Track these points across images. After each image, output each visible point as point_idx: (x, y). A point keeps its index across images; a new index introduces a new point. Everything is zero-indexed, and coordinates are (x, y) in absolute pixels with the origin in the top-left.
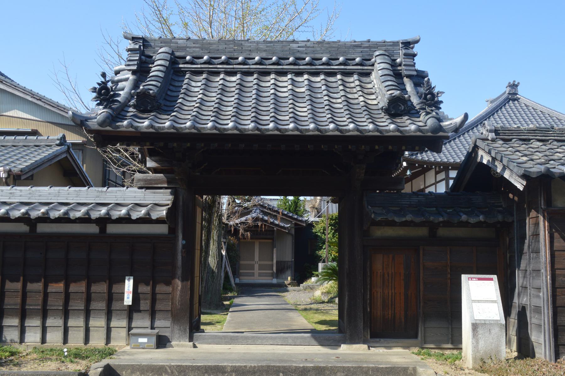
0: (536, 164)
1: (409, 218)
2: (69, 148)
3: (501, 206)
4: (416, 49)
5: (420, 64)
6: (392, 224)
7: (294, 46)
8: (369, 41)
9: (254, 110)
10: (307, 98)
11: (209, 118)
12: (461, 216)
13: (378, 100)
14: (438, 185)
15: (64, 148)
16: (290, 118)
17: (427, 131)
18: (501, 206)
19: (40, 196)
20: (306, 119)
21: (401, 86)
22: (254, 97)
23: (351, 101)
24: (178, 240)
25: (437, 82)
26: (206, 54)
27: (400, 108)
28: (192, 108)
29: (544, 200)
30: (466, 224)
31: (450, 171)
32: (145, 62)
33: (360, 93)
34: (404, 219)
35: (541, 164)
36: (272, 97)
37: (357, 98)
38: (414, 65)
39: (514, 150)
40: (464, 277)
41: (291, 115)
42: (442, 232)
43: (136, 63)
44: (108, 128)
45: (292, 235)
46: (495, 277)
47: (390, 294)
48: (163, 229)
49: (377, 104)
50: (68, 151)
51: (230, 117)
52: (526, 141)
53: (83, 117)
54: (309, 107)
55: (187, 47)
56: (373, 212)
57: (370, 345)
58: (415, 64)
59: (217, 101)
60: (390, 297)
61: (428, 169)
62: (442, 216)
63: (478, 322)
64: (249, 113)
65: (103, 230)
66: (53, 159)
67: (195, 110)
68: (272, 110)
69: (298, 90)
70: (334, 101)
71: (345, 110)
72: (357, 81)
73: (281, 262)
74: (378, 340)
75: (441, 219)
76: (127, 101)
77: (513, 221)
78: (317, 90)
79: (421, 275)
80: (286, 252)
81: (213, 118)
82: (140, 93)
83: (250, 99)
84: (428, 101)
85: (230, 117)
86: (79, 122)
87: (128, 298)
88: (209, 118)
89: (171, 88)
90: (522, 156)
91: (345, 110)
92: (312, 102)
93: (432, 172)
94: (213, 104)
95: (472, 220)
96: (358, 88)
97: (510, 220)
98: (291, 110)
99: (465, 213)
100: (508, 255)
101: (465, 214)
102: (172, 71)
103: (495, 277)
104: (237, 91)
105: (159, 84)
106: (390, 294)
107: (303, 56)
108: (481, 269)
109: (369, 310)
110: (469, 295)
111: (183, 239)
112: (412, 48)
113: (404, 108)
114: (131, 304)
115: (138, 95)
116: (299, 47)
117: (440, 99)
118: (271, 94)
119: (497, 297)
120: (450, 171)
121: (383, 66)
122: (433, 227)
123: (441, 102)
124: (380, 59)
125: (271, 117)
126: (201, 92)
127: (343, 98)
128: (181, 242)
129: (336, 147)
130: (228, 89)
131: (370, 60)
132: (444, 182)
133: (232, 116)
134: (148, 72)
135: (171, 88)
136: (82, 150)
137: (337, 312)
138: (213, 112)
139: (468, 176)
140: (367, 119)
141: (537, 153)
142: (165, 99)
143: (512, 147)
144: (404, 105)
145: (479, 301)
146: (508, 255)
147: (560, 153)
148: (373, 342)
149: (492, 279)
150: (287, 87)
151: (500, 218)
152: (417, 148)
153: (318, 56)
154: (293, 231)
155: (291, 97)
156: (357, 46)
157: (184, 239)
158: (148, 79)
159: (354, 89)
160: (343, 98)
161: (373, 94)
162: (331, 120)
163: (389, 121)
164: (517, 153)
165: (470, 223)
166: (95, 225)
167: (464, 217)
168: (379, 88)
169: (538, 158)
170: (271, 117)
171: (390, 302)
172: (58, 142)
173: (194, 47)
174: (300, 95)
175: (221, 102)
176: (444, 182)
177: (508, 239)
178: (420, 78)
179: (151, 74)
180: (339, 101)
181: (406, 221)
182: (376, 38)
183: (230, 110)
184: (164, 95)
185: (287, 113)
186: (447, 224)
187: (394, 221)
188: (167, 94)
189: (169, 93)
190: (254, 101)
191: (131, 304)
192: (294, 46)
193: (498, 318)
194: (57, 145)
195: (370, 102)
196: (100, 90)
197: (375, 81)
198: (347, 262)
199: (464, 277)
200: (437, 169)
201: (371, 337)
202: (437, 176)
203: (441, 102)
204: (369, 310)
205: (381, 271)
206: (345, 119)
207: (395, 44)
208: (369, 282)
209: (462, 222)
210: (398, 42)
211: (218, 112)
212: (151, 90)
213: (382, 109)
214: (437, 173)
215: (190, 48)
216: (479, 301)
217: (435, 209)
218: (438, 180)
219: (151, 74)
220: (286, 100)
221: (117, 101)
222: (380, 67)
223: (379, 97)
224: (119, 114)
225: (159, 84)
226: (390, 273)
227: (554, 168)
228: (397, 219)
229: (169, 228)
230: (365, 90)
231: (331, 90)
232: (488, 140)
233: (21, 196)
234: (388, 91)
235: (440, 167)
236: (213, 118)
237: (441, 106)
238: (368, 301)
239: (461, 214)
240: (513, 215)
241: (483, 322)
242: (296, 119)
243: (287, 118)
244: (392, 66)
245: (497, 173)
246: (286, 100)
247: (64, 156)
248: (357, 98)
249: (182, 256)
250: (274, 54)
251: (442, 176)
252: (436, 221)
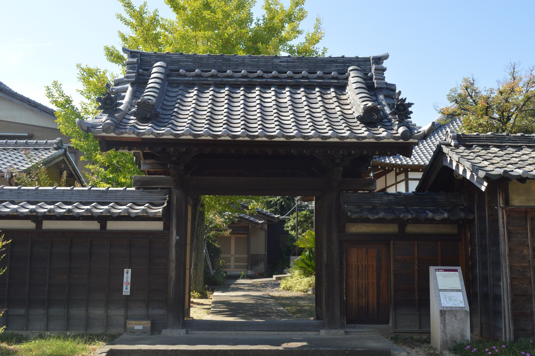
0: (496, 168)
1: (381, 215)
2: (65, 151)
3: (463, 205)
4: (385, 64)
5: (389, 78)
6: (366, 221)
7: (277, 61)
8: (343, 57)
9: (243, 118)
10: (290, 107)
11: (203, 125)
12: (427, 214)
13: (353, 110)
14: (398, 185)
15: (61, 151)
16: (276, 125)
17: (398, 138)
18: (463, 205)
19: (46, 196)
20: (290, 126)
21: (376, 100)
22: (242, 106)
23: (330, 111)
24: (172, 236)
25: (406, 93)
26: (197, 68)
27: (374, 117)
28: (187, 116)
29: (503, 200)
30: (432, 221)
31: (409, 173)
32: (142, 75)
33: (337, 104)
34: (376, 217)
35: (500, 168)
36: (258, 106)
37: (334, 108)
38: (384, 79)
39: (475, 155)
40: (432, 269)
41: (277, 123)
42: (411, 229)
43: (134, 74)
44: (112, 135)
45: (265, 230)
46: (459, 268)
47: (364, 284)
48: (158, 226)
49: (352, 114)
50: (65, 154)
51: (221, 125)
52: (486, 147)
53: (90, 124)
54: (292, 116)
55: (180, 61)
56: (349, 210)
57: (346, 330)
58: (384, 77)
59: (209, 110)
60: (364, 287)
61: (389, 171)
62: (411, 214)
63: (445, 309)
64: (239, 121)
65: (103, 226)
66: (51, 161)
67: (190, 118)
68: (259, 119)
69: (281, 100)
70: (314, 110)
71: (324, 119)
72: (334, 93)
73: (255, 255)
74: (353, 325)
75: (410, 217)
76: (127, 110)
77: (474, 219)
78: (297, 101)
79: (392, 267)
80: (259, 245)
81: (207, 126)
82: (140, 102)
83: (238, 109)
84: (400, 111)
85: (221, 125)
86: (86, 129)
87: (126, 289)
88: (203, 125)
89: (167, 98)
90: (483, 161)
91: (324, 119)
92: (295, 113)
93: (393, 173)
94: (205, 112)
95: (438, 217)
96: (335, 99)
97: (471, 217)
98: (276, 119)
99: (431, 211)
100: (470, 249)
101: (431, 212)
102: (167, 82)
103: (459, 268)
104: (226, 101)
105: (156, 95)
106: (364, 284)
107: (285, 69)
108: (448, 262)
109: (345, 298)
110: (437, 285)
111: (177, 235)
112: (382, 63)
113: (378, 117)
114: (129, 294)
115: (138, 104)
116: (281, 62)
117: (410, 109)
118: (257, 104)
119: (462, 286)
120: (409, 173)
121: (356, 79)
122: (402, 224)
123: (411, 112)
124: (354, 73)
125: (259, 125)
126: (194, 101)
127: (322, 108)
128: (175, 237)
129: (317, 152)
130: (218, 100)
131: (345, 74)
132: (404, 183)
133: (224, 124)
134: (146, 83)
135: (167, 98)
136: (75, 153)
137: (191, 311)
138: (206, 120)
139: (433, 177)
140: (345, 127)
141: (496, 158)
142: (162, 108)
143: (473, 152)
144: (377, 115)
145: (445, 290)
146: (470, 249)
147: (516, 157)
148: (349, 328)
149: (456, 271)
150: (271, 98)
151: (462, 215)
152: (389, 153)
153: (298, 70)
154: (266, 227)
155: (275, 107)
156: (332, 61)
157: (177, 234)
158: (146, 90)
159: (331, 100)
160: (322, 108)
161: (348, 104)
162: (312, 128)
163: (364, 129)
164: (478, 158)
165: (435, 220)
166: (96, 222)
167: (430, 215)
168: (353, 99)
169: (496, 162)
170: (259, 125)
171: (364, 292)
172: (55, 146)
173: (187, 61)
174: (283, 105)
175: (213, 112)
176: (404, 183)
177: (469, 235)
178: (390, 91)
179: (148, 86)
180: (318, 110)
181: (379, 219)
182: (350, 54)
183: (222, 118)
184: (161, 104)
185: (273, 121)
186: (416, 221)
187: (368, 218)
188: (163, 104)
189: (165, 102)
190: (242, 110)
191: (129, 294)
192: (277, 61)
193: (462, 305)
194: (56, 149)
195: (346, 111)
196: (106, 99)
197: (349, 92)
198: (325, 256)
199: (432, 269)
200: (398, 171)
201: (347, 324)
202: (398, 177)
203: (411, 112)
204: (345, 298)
205: (356, 263)
206: (324, 127)
207: (367, 60)
208: (345, 273)
209: (428, 219)
210: (369, 58)
211: (211, 120)
212: (150, 100)
213: (358, 118)
214: (397, 174)
215: (183, 62)
216: (445, 290)
217: (403, 207)
218: (398, 181)
219: (148, 86)
220: (271, 109)
221: (120, 110)
222: (353, 80)
223: (354, 107)
224: (121, 121)
225: (156, 95)
226: (364, 265)
227: (512, 171)
228: (370, 217)
229: (164, 223)
230: (342, 101)
231: (311, 101)
232: (451, 146)
233: (28, 195)
234: (363, 102)
235: (400, 169)
236: (207, 126)
237: (411, 115)
238: (345, 291)
239: (428, 212)
240: (474, 213)
241: (450, 309)
242: (281, 126)
243: (273, 126)
244: (364, 79)
245: (459, 175)
246: (271, 109)
247: (62, 158)
248: (334, 108)
249: (176, 250)
250: (258, 68)
251: (402, 177)
252: (406, 219)
